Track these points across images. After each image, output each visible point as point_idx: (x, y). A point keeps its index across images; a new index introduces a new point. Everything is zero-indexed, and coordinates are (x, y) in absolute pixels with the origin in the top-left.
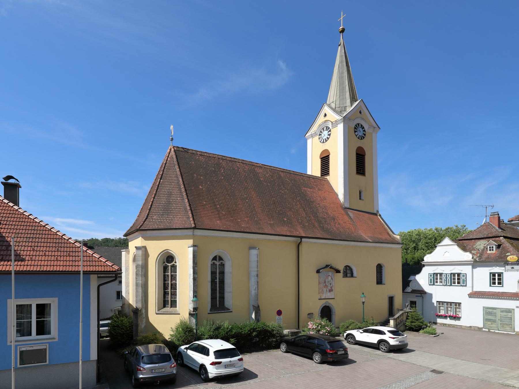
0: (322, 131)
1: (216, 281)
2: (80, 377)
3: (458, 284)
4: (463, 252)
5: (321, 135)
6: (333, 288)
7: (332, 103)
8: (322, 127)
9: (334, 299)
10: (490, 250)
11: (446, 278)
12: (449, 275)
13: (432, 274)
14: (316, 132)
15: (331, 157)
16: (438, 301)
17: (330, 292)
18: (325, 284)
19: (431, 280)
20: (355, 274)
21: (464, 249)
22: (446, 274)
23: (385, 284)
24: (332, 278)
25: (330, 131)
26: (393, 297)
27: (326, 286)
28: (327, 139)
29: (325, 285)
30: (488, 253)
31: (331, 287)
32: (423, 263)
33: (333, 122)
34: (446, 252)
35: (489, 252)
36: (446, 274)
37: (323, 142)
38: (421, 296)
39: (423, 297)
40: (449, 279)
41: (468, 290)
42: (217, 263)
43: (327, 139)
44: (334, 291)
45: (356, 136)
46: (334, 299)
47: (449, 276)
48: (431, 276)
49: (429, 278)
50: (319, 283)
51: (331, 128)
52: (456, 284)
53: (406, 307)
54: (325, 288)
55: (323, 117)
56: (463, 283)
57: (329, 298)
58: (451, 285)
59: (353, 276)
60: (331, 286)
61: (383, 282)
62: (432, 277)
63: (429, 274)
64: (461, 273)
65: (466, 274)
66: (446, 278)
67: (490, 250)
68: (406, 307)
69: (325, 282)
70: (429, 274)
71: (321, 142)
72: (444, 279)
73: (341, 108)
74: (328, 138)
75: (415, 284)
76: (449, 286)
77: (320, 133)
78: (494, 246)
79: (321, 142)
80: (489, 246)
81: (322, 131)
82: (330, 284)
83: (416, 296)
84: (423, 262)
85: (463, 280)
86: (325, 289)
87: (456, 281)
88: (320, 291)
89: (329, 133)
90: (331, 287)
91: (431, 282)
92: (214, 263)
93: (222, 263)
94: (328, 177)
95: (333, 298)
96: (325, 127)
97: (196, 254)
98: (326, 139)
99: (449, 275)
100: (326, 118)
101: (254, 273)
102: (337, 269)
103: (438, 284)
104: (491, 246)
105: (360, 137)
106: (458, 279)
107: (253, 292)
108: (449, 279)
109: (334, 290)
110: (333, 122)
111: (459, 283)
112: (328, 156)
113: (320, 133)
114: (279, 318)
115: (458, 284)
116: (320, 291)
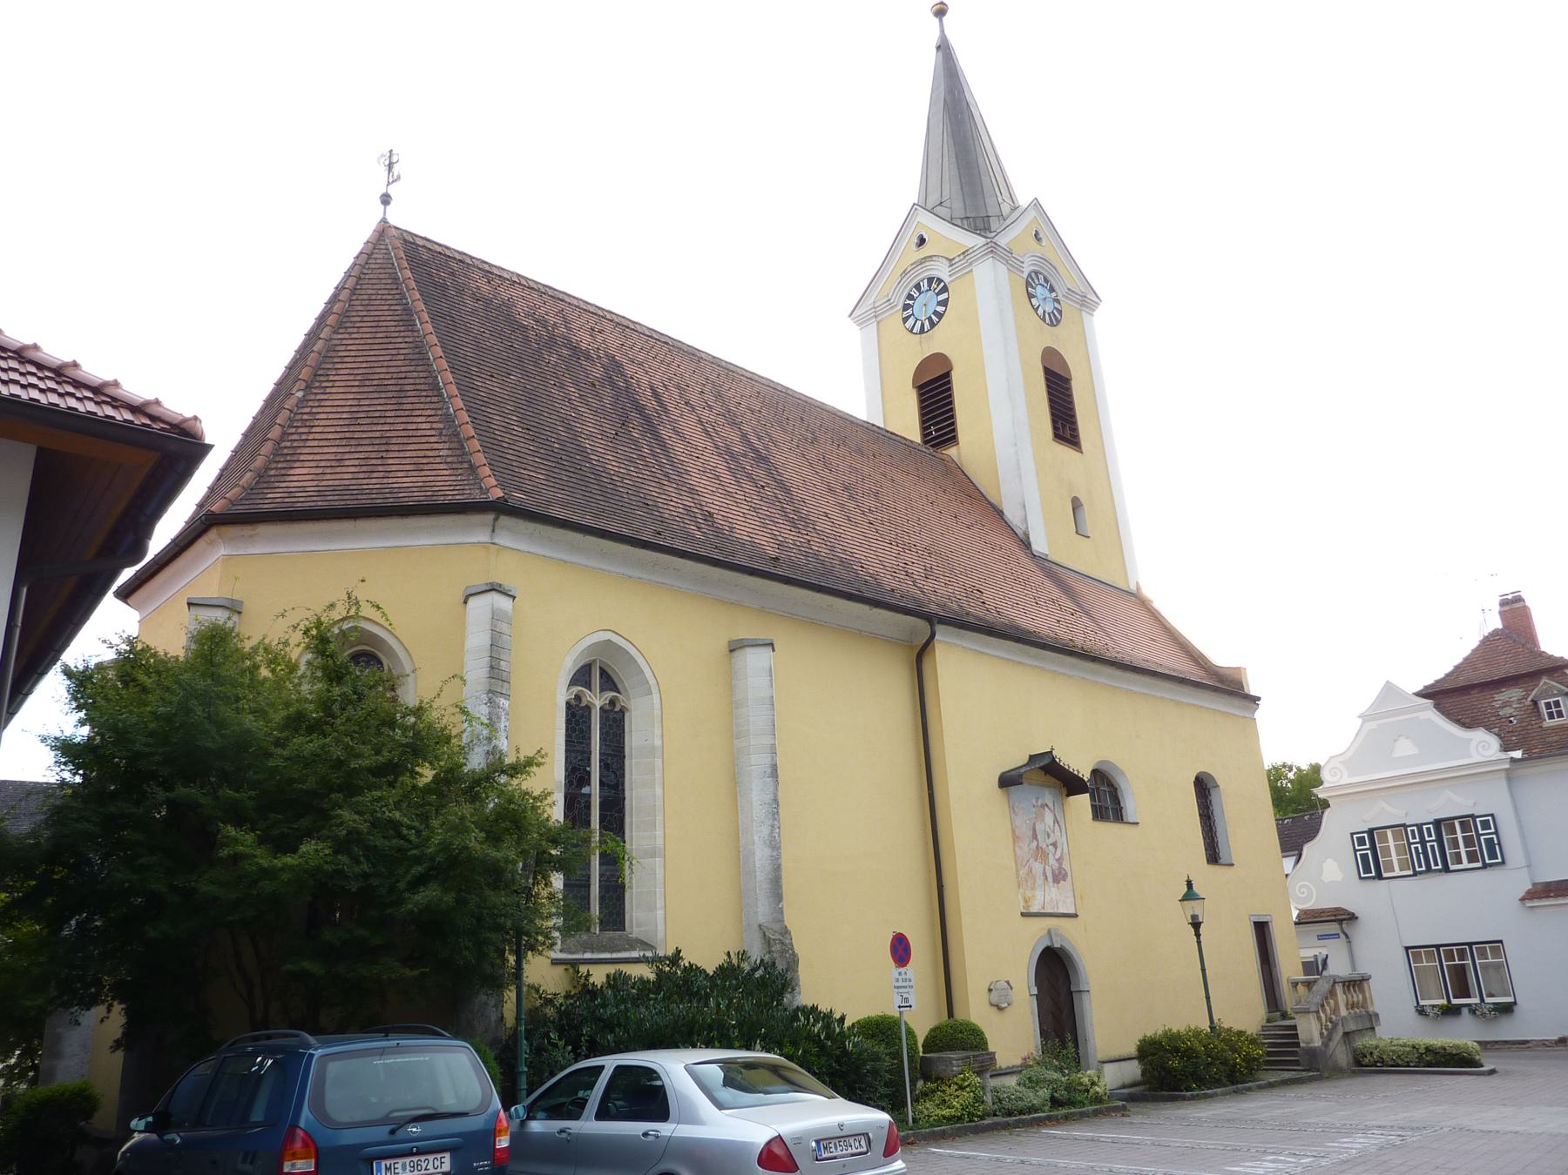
0: (912, 293)
1: (585, 790)
2: (10, 677)
3: (1470, 861)
4: (1461, 732)
5: (912, 306)
6: (1066, 866)
7: (939, 208)
8: (908, 287)
9: (1075, 916)
10: (1551, 716)
11: (1423, 842)
12: (1428, 829)
13: (1365, 835)
14: (889, 300)
15: (956, 377)
16: (1407, 945)
17: (1058, 883)
18: (1035, 843)
19: (1364, 857)
20: (1131, 806)
21: (1467, 721)
22: (1420, 826)
23: (1233, 865)
24: (1056, 821)
25: (945, 289)
26: (1267, 922)
27: (1040, 854)
28: (933, 317)
29: (1037, 847)
30: (1548, 728)
31: (1059, 860)
32: (1321, 793)
33: (953, 259)
34: (1400, 736)
35: (1548, 723)
36: (1416, 825)
37: (922, 331)
38: (1336, 936)
39: (1347, 937)
40: (1432, 847)
41: (1512, 881)
42: (597, 700)
43: (933, 317)
44: (1070, 877)
45: (1036, 310)
46: (1075, 916)
47: (1430, 835)
48: (1361, 841)
49: (1355, 851)
50: (1016, 838)
51: (946, 279)
52: (1465, 864)
53: (1320, 968)
54: (1036, 860)
55: (914, 247)
56: (1493, 855)
57: (1056, 911)
58: (1446, 869)
59: (1125, 820)
60: (1057, 857)
61: (1221, 855)
62: (1368, 846)
63: (1352, 834)
64: (1473, 817)
65: (1492, 815)
66: (1423, 842)
67: (1551, 716)
68: (1320, 968)
69: (1035, 837)
70: (1352, 834)
71: (915, 331)
72: (1416, 849)
73: (971, 220)
74: (940, 316)
75: (1304, 886)
76: (1440, 871)
77: (908, 302)
78: (1559, 698)
79: (911, 331)
80: (1543, 702)
81: (915, 293)
82: (1055, 845)
83: (1321, 937)
84: (1321, 787)
85: (1489, 842)
86: (1038, 867)
87: (1463, 850)
88: (1023, 872)
89: (943, 297)
90: (1059, 860)
91: (1367, 870)
92: (578, 697)
93: (612, 702)
94: (952, 452)
95: (1072, 911)
96: (926, 281)
97: (504, 627)
98: (930, 319)
99: (1428, 829)
100: (926, 251)
101: (757, 762)
102: (1076, 773)
103: (1397, 872)
104: (1551, 700)
105: (1047, 316)
106: (1468, 842)
107: (761, 856)
108: (1432, 847)
109: (1069, 874)
110: (953, 259)
111: (1472, 857)
112: (947, 375)
113: (908, 302)
114: (900, 978)
115: (1470, 861)
116: (1021, 873)
